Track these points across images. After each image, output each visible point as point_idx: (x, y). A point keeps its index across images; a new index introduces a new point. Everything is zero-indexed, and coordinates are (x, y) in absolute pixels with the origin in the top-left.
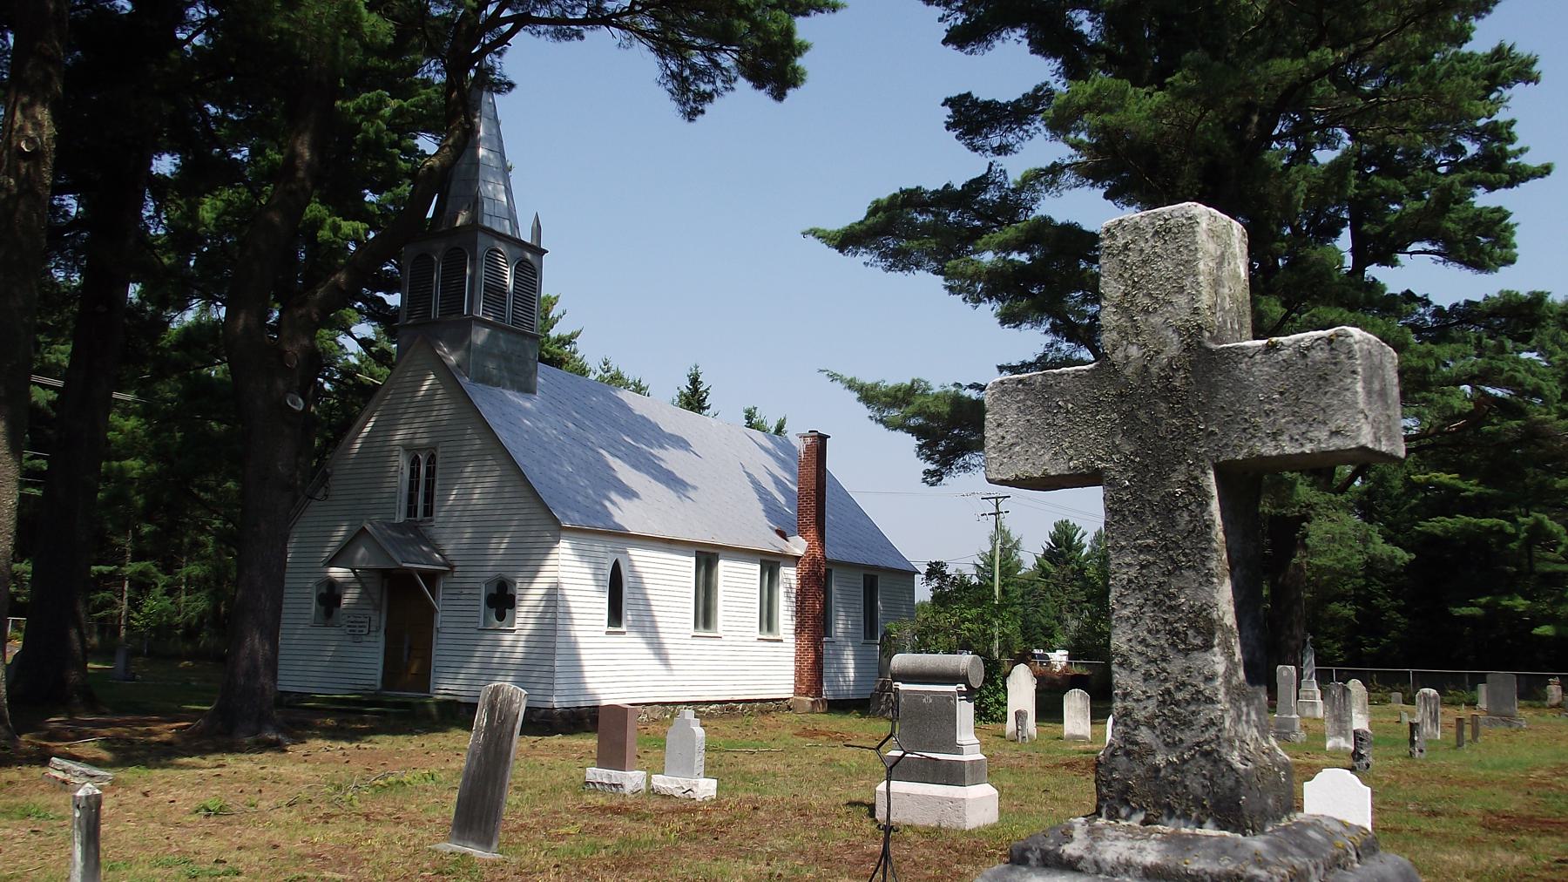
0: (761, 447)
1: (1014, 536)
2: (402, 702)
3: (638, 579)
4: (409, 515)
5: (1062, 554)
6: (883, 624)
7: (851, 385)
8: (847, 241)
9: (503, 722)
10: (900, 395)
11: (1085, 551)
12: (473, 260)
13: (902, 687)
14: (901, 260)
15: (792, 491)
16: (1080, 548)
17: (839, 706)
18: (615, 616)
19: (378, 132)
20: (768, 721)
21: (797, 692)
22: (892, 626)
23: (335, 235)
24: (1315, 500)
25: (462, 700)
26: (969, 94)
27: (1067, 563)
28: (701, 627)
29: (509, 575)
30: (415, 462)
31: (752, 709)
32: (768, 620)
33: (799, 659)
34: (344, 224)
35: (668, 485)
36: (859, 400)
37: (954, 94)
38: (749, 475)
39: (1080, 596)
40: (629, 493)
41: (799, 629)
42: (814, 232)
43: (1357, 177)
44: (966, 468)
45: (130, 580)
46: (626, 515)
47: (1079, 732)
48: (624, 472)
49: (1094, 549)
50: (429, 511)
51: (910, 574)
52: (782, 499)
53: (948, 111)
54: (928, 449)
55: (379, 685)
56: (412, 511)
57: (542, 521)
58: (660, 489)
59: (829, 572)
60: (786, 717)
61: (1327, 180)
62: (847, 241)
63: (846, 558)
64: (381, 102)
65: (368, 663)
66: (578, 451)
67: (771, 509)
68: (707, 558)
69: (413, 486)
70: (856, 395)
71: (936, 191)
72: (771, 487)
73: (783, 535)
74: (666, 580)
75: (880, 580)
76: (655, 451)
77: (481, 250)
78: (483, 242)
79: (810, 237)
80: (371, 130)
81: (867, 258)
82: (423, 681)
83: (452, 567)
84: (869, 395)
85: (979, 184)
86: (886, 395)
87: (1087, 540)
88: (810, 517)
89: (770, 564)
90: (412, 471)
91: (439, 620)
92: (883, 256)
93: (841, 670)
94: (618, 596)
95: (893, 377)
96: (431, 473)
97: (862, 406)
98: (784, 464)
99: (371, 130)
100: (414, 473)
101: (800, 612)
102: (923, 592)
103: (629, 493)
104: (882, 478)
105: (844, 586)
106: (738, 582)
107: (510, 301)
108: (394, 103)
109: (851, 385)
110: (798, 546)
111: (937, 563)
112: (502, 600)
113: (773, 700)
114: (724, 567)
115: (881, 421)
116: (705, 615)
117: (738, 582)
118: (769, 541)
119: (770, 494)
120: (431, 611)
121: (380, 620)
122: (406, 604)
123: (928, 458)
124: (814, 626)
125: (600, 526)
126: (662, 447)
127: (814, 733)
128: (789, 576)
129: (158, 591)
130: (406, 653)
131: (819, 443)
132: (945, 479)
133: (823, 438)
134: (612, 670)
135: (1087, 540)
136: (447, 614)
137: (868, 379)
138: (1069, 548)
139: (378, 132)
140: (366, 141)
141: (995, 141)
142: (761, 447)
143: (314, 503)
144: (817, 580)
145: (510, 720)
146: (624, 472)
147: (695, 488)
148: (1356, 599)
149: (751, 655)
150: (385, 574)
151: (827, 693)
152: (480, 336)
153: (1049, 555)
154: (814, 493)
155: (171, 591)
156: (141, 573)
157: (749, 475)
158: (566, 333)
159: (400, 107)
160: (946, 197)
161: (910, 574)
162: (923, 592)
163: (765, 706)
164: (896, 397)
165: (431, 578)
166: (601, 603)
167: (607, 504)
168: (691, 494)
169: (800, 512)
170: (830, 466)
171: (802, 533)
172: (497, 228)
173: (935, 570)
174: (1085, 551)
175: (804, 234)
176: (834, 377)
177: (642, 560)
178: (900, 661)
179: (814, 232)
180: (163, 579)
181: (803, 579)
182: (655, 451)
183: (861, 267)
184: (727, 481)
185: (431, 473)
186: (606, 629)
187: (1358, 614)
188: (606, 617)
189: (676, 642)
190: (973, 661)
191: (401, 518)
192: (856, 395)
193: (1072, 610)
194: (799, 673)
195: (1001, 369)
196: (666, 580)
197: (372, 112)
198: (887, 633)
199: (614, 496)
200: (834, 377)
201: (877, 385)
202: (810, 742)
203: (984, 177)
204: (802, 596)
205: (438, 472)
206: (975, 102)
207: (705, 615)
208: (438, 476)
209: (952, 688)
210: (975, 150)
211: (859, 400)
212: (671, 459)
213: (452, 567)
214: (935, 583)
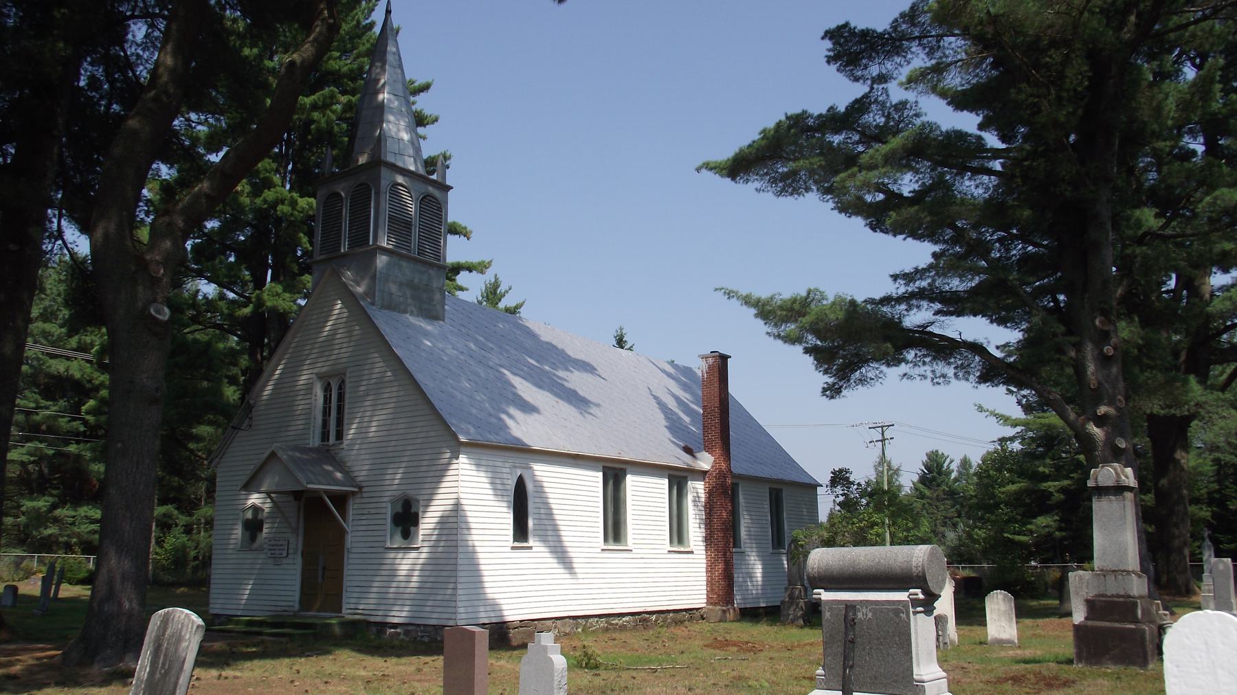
0: (664, 371)
1: (895, 465)
2: (315, 623)
3: (539, 487)
4: (323, 440)
5: (934, 479)
6: (790, 531)
7: (747, 301)
8: (738, 167)
9: (167, 673)
10: (796, 306)
11: (953, 475)
12: (378, 193)
13: (826, 596)
14: (789, 185)
15: (697, 413)
16: (949, 473)
17: (750, 614)
18: (521, 531)
19: (329, 123)
20: (679, 631)
21: (710, 601)
22: (799, 533)
23: (294, 208)
24: (1203, 399)
25: (372, 619)
26: (846, 25)
27: (938, 485)
28: (611, 540)
29: (411, 492)
30: (327, 389)
31: (665, 620)
32: (678, 533)
33: (710, 568)
34: (300, 200)
35: (570, 402)
36: (756, 316)
37: (833, 25)
38: (656, 398)
39: (952, 512)
40: (528, 408)
41: (709, 540)
42: (708, 166)
43: (1222, 90)
44: (862, 381)
45: (158, 521)
46: (523, 428)
47: (1005, 636)
48: (524, 388)
49: (960, 473)
50: (340, 436)
51: (812, 487)
52: (687, 419)
53: (828, 44)
54: (822, 357)
55: (297, 607)
56: (325, 436)
57: (436, 433)
58: (565, 408)
59: (735, 487)
60: (697, 627)
61: (1193, 95)
62: (738, 167)
63: (752, 473)
64: (332, 99)
65: (286, 585)
66: (481, 371)
67: (675, 426)
68: (614, 475)
69: (326, 412)
70: (753, 311)
71: (820, 116)
72: (672, 404)
73: (688, 450)
74: (572, 495)
75: (785, 494)
76: (561, 373)
77: (384, 183)
78: (386, 176)
79: (704, 171)
80: (323, 120)
81: (757, 185)
82: (335, 603)
83: (361, 488)
84: (767, 311)
85: (860, 106)
86: (781, 308)
87: (954, 466)
88: (715, 434)
89: (678, 480)
90: (325, 397)
91: (349, 540)
92: (774, 181)
93: (750, 576)
94: (523, 507)
95: (787, 288)
96: (341, 397)
97: (760, 322)
98: (685, 387)
99: (323, 120)
100: (327, 400)
101: (709, 523)
102: (826, 503)
103: (528, 408)
104: (785, 399)
105: (748, 499)
106: (646, 497)
107: (415, 232)
108: (344, 99)
109: (747, 301)
110: (705, 461)
111: (841, 471)
112: (406, 519)
113: (686, 610)
114: (632, 482)
115: (779, 336)
116: (614, 528)
117: (646, 497)
118: (678, 459)
119: (676, 414)
120: (342, 533)
121: (297, 542)
122: (319, 520)
123: (826, 372)
124: (724, 539)
125: (493, 438)
126: (568, 370)
127: (723, 644)
128: (697, 489)
129: (177, 531)
130: (320, 574)
131: (721, 364)
132: (844, 392)
133: (723, 359)
134: (516, 582)
135: (954, 466)
136: (358, 530)
137: (763, 293)
138: (940, 473)
139: (329, 123)
140: (319, 130)
141: (874, 70)
142: (664, 371)
143: (241, 433)
144: (725, 495)
145: (177, 665)
146: (524, 388)
147: (598, 405)
148: (1211, 502)
149: (661, 567)
150: (297, 495)
151: (738, 601)
152: (381, 260)
153: (923, 480)
154: (715, 410)
155: (188, 530)
156: (165, 515)
157: (656, 398)
158: (512, 304)
159: (350, 101)
160: (835, 121)
161: (812, 487)
162: (826, 503)
163: (679, 616)
164: (792, 309)
165: (341, 500)
166: (506, 518)
167: (504, 416)
168: (593, 410)
169: (705, 428)
170: (732, 390)
171: (708, 449)
172: (400, 164)
173: (840, 478)
174: (953, 475)
175: (698, 170)
176: (730, 294)
177: (542, 471)
178: (820, 558)
179: (708, 166)
180: (183, 519)
181: (710, 494)
182: (561, 373)
183: (751, 194)
184: (637, 409)
185: (341, 397)
186: (511, 543)
187: (1214, 515)
188: (511, 532)
189: (575, 550)
190: (932, 554)
191: (315, 441)
192: (753, 311)
193: (945, 524)
194: (710, 583)
195: (895, 277)
196: (572, 495)
197: (324, 106)
198: (795, 540)
199: (512, 410)
200: (730, 294)
201: (772, 298)
202: (720, 654)
203: (866, 96)
204: (710, 509)
205: (347, 396)
206: (852, 32)
207: (614, 528)
208: (347, 401)
209: (902, 596)
210: (856, 79)
211: (756, 316)
212: (576, 380)
213: (361, 488)
214: (839, 490)
